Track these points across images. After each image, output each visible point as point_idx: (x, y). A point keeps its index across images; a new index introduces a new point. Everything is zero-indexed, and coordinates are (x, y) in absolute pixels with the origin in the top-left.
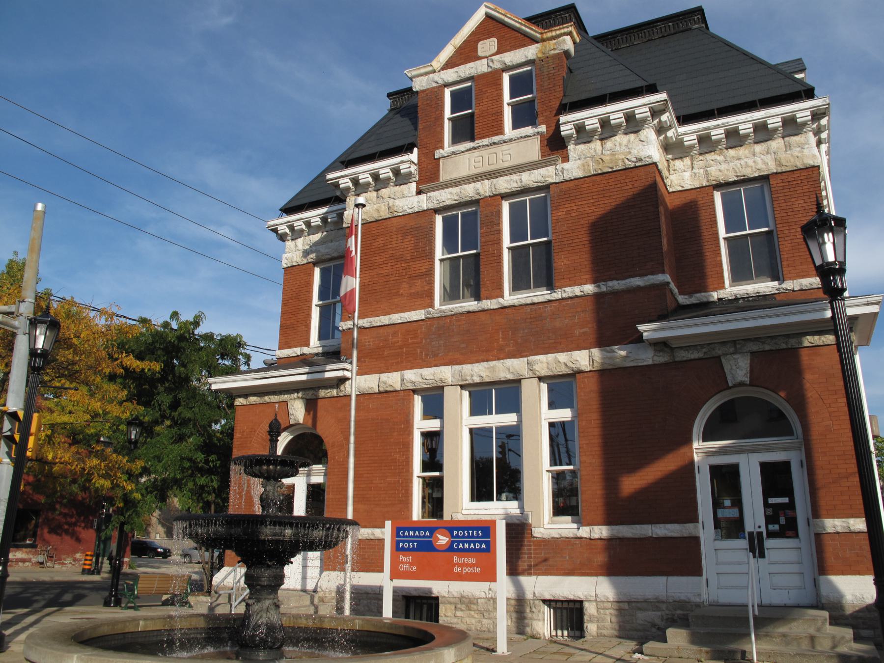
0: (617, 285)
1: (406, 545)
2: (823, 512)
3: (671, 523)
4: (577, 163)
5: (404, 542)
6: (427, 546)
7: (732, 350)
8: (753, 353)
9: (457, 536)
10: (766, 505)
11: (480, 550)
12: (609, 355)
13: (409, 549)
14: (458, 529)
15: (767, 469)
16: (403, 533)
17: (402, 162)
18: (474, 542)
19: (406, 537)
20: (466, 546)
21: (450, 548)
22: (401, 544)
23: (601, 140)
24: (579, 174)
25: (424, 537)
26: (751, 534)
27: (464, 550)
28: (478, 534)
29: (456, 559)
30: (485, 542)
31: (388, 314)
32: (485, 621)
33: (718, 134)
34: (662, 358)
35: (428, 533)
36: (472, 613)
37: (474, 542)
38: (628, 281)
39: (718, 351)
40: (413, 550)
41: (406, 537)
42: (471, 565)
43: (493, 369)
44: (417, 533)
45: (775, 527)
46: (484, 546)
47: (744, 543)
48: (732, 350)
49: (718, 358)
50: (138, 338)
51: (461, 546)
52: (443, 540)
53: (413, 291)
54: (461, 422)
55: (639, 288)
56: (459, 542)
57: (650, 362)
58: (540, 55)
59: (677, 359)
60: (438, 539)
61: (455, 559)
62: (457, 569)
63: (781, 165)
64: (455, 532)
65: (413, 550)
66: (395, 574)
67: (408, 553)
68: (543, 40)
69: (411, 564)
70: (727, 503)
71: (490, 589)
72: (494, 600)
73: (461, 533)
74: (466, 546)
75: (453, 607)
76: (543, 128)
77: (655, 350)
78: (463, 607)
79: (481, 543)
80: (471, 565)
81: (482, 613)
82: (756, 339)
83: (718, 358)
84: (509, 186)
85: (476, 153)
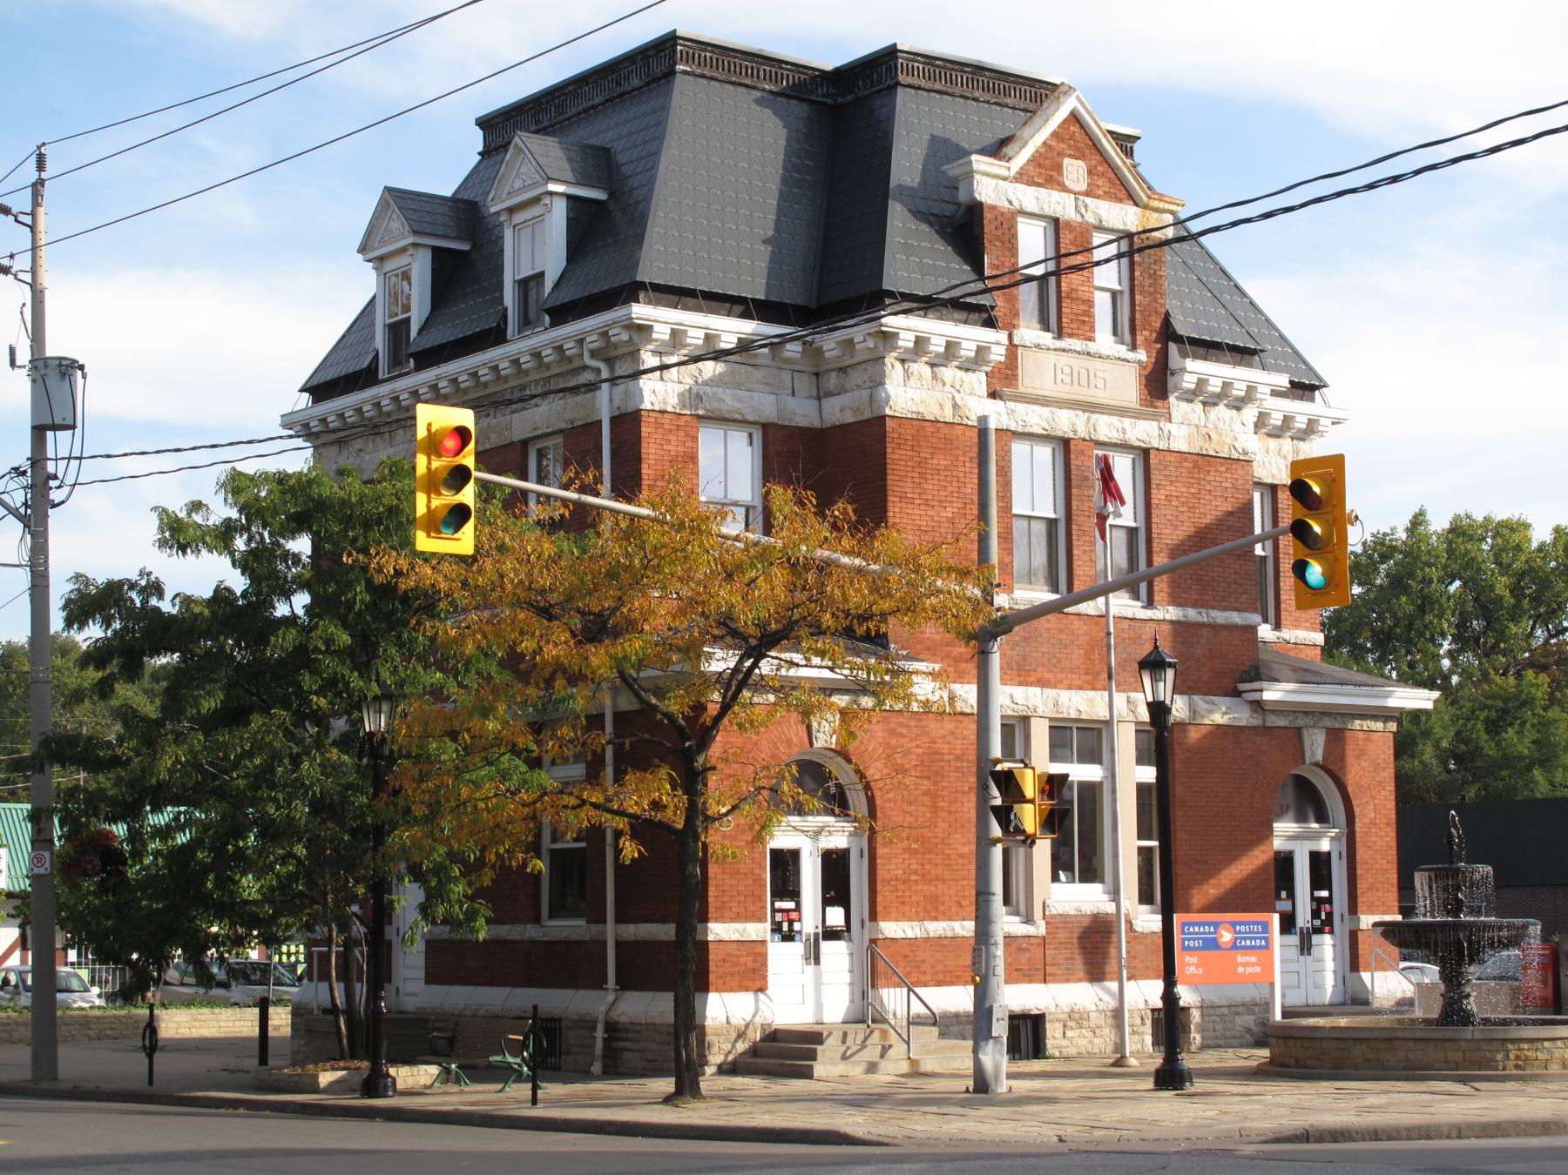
0: (1192, 614)
2: (879, 915)
4: (1180, 428)
10: (1313, 898)
11: (1260, 947)
13: (1194, 949)
21: (1234, 946)
23: (1204, 404)
26: (808, 935)
27: (1246, 948)
38: (1228, 614)
39: (1300, 722)
40: (1199, 948)
42: (1253, 965)
43: (1091, 702)
45: (1317, 923)
49: (1299, 729)
50: (854, 528)
55: (1236, 627)
61: (1240, 959)
65: (1199, 948)
68: (1146, 207)
69: (1197, 966)
70: (1284, 894)
75: (1060, 1026)
76: (1142, 355)
78: (1072, 1024)
80: (1253, 965)
83: (1299, 729)
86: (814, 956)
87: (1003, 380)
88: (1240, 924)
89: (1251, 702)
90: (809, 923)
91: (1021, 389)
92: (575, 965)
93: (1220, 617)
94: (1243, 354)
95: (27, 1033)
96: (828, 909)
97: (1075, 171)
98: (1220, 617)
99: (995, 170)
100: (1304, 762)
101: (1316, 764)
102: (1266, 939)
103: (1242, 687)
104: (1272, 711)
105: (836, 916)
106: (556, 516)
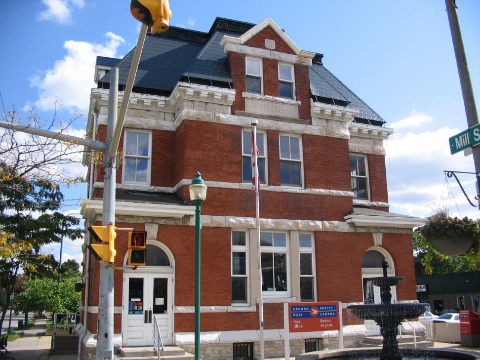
1: (297, 315)
3: (218, 305)
5: (295, 313)
6: (307, 315)
7: (376, 231)
8: (383, 233)
9: (322, 310)
12: (332, 225)
14: (296, 307)
15: (156, 281)
16: (295, 309)
17: (231, 94)
18: (330, 312)
19: (297, 311)
20: (326, 314)
21: (318, 316)
22: (294, 315)
24: (317, 133)
25: (306, 310)
26: (146, 312)
27: (325, 316)
28: (295, 309)
29: (295, 321)
30: (335, 312)
31: (216, 181)
32: (279, 352)
33: (365, 131)
34: (352, 230)
35: (307, 309)
36: (272, 349)
37: (327, 312)
38: (339, 191)
39: (372, 230)
41: (297, 311)
42: (329, 323)
44: (297, 309)
46: (334, 314)
47: (142, 316)
48: (376, 231)
51: (323, 314)
52: (315, 312)
53: (231, 170)
54: (253, 251)
56: (322, 313)
57: (347, 231)
58: (298, 62)
59: (357, 232)
60: (313, 312)
62: (322, 326)
63: (374, 151)
64: (321, 308)
65: (301, 317)
66: (292, 330)
67: (329, 318)
69: (299, 324)
71: (281, 336)
72: (283, 341)
73: (323, 308)
74: (326, 314)
77: (350, 226)
79: (332, 312)
80: (329, 323)
81: (277, 348)
82: (384, 228)
84: (288, 128)
85: (265, 103)
86: (148, 319)
87: (238, 106)
88: (322, 306)
89: (349, 223)
90: (148, 305)
91: (246, 112)
92: (363, 314)
93: (334, 192)
94: (344, 104)
95: (2, 330)
96: (156, 299)
97: (270, 43)
98: (334, 192)
99: (235, 41)
100: (374, 245)
101: (380, 246)
102: (335, 312)
103: (345, 218)
104: (359, 227)
105: (160, 301)
106: (37, 280)
